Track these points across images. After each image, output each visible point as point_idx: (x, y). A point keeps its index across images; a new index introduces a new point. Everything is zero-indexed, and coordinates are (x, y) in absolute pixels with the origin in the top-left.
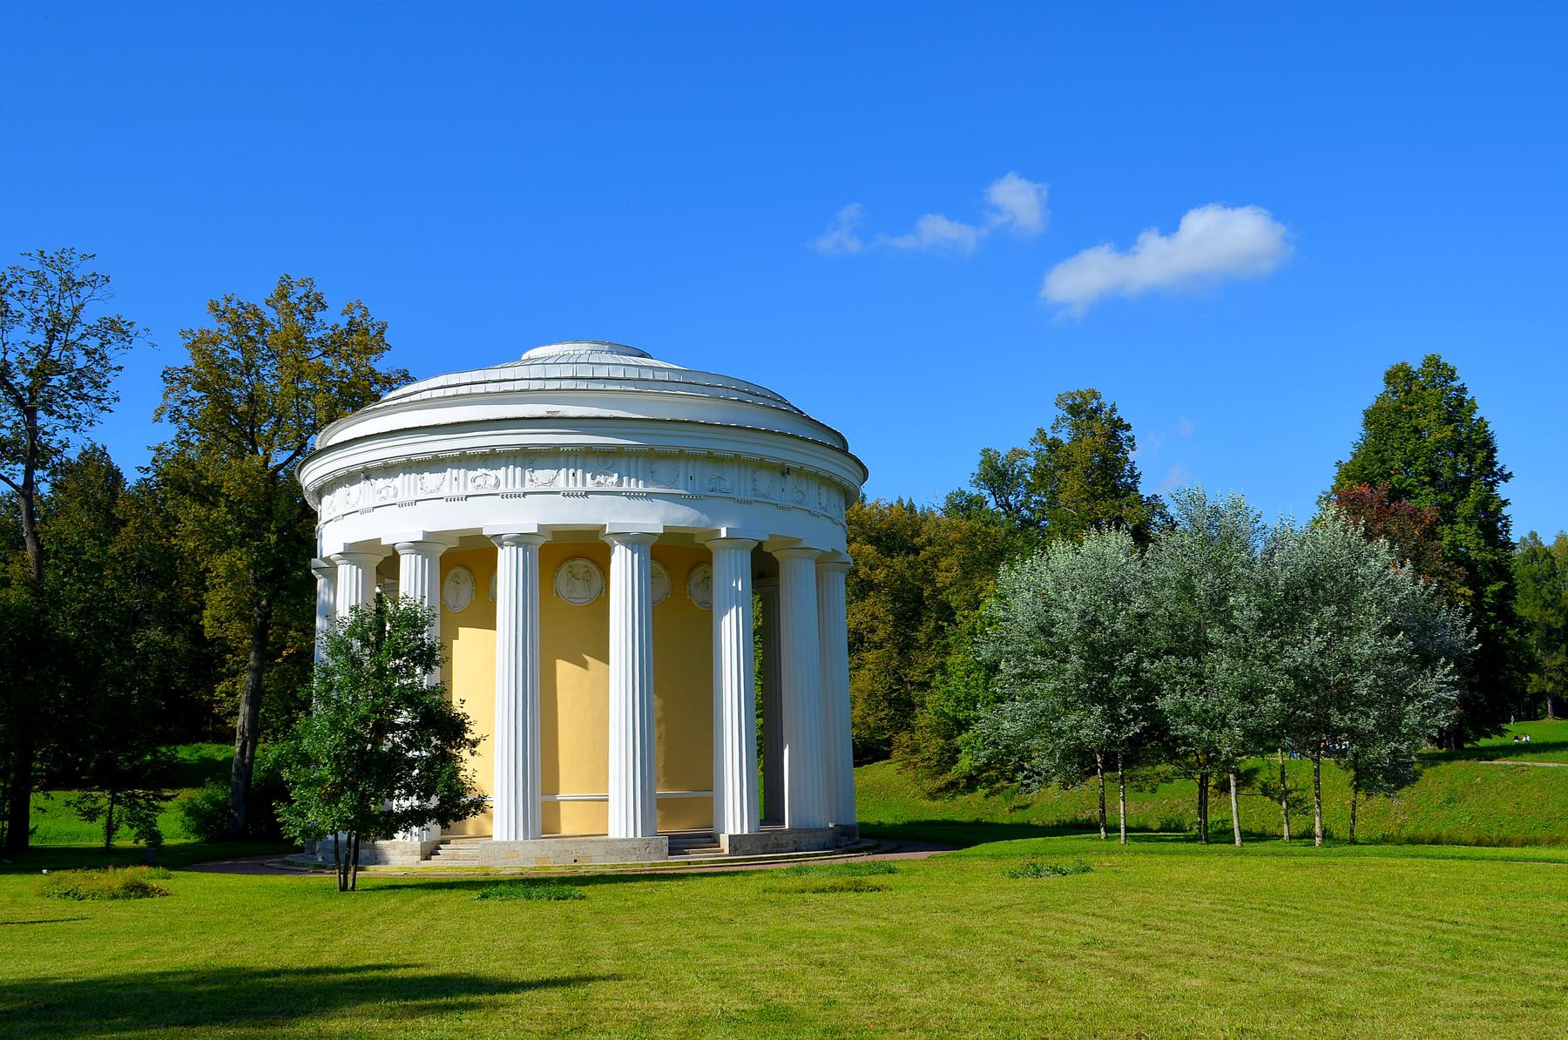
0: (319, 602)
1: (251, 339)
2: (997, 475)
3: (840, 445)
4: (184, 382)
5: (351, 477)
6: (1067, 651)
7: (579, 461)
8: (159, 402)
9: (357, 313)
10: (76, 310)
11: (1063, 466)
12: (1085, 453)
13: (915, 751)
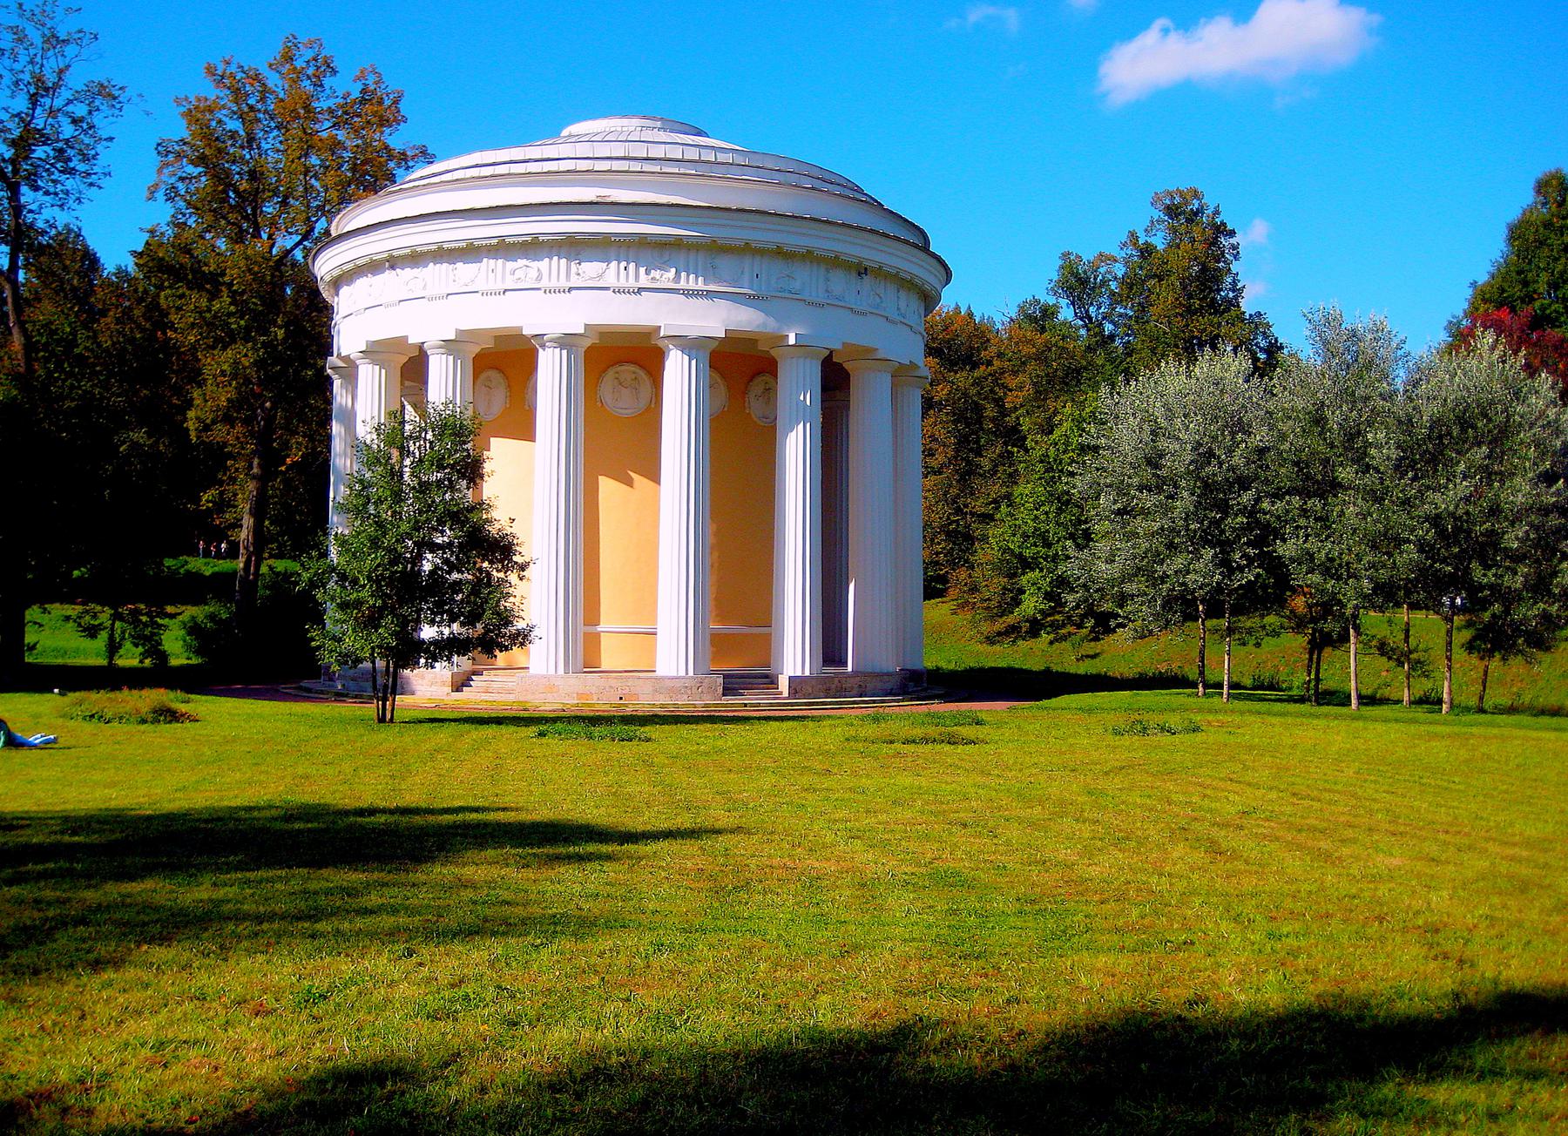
0: (335, 406)
1: (251, 108)
2: (1077, 283)
3: (920, 241)
4: (179, 156)
5: (373, 267)
6: (1176, 486)
7: (631, 254)
8: (152, 178)
9: (371, 79)
10: (61, 71)
11: (1155, 276)
12: (1184, 263)
13: (974, 589)
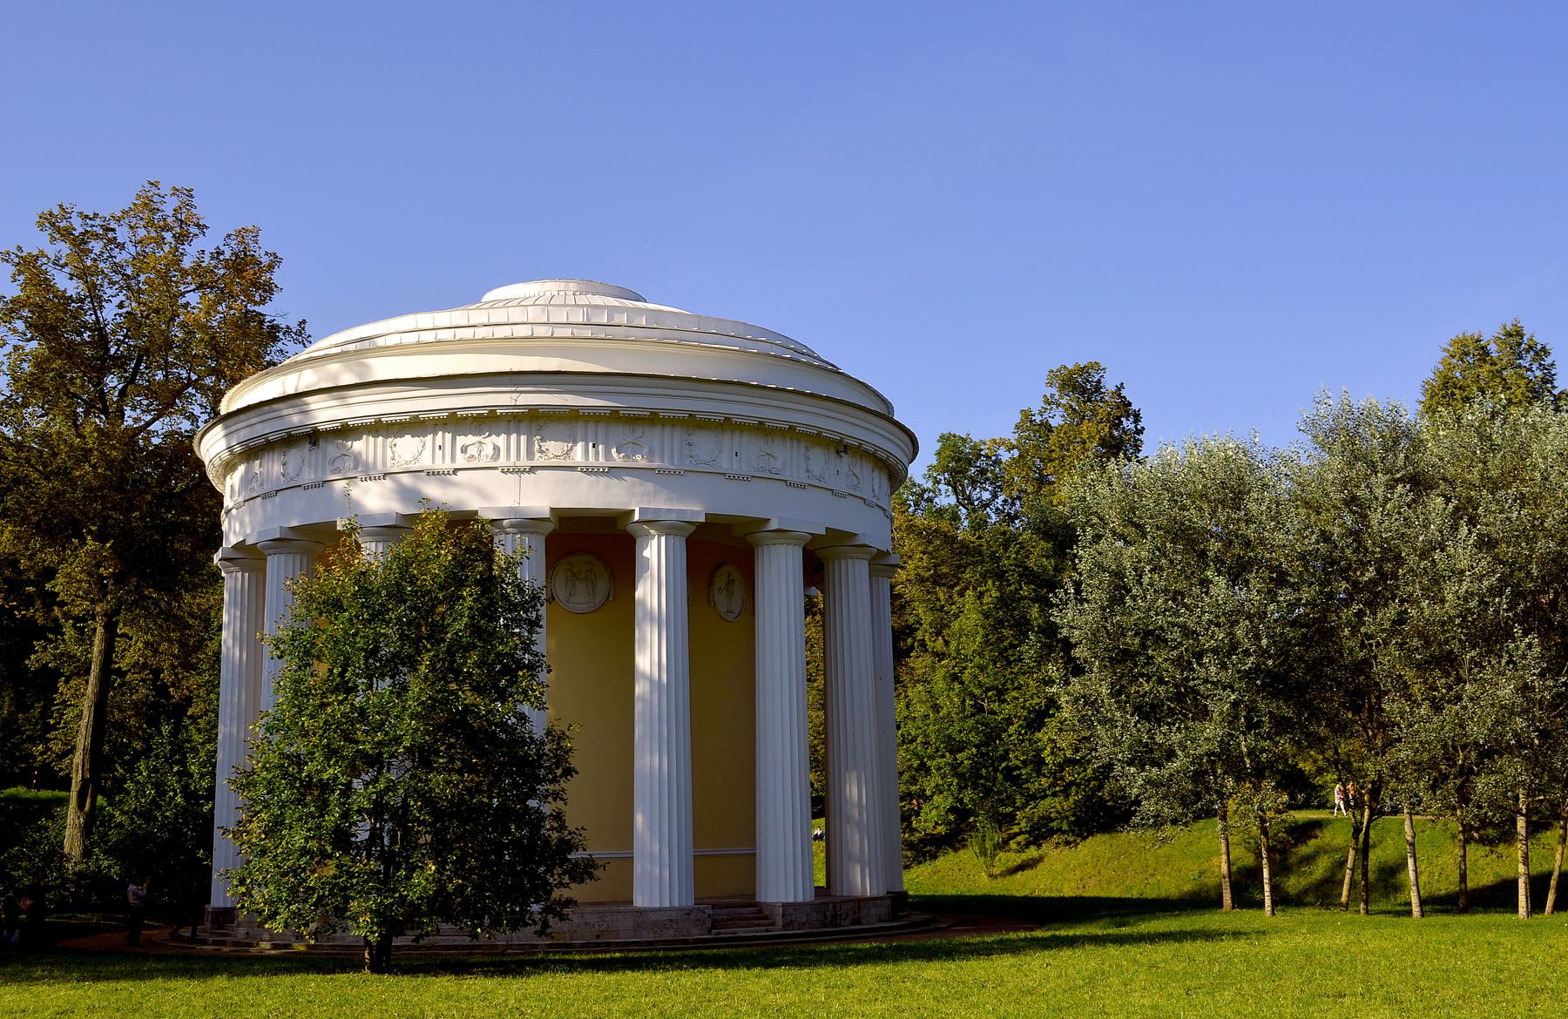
3: (884, 414)
